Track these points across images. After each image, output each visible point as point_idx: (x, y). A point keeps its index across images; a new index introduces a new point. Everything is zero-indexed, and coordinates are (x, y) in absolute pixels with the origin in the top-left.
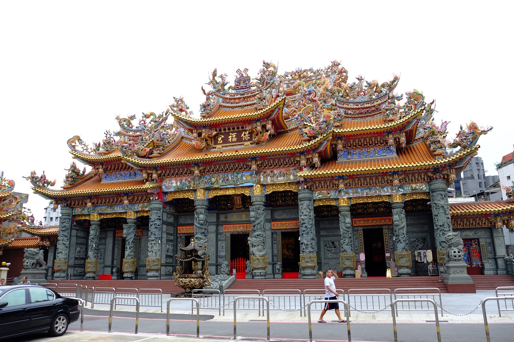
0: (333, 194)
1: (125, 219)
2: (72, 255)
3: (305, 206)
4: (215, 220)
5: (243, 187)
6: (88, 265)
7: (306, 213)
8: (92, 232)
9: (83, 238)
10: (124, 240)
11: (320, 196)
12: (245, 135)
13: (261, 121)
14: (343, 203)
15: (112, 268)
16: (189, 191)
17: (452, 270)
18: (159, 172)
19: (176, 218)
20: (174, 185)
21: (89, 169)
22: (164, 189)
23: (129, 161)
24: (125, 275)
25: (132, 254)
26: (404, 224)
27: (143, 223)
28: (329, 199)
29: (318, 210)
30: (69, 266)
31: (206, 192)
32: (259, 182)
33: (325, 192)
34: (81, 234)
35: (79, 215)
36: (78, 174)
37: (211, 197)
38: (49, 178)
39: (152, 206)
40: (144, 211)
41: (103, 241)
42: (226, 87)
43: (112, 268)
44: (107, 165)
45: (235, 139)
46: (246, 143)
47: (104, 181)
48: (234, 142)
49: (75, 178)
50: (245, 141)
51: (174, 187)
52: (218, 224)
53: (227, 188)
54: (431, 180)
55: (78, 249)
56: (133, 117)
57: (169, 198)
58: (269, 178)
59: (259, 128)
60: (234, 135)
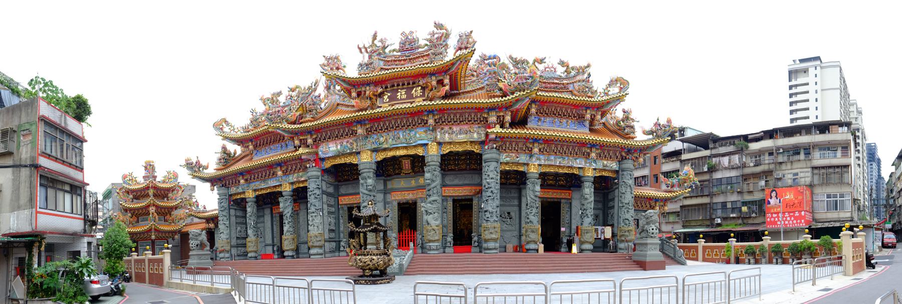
0: (523, 158)
1: (281, 193)
2: (234, 235)
3: (492, 168)
4: (382, 188)
5: (415, 146)
6: (248, 244)
7: (491, 176)
8: (249, 210)
9: (243, 217)
10: (281, 217)
14: (533, 170)
15: (273, 246)
16: (351, 154)
17: (649, 246)
19: (337, 188)
22: (321, 155)
23: (278, 128)
24: (286, 254)
25: (291, 229)
26: (592, 199)
27: (300, 195)
28: (518, 164)
29: (505, 175)
30: (231, 247)
31: (374, 154)
32: (435, 140)
34: (239, 213)
35: (235, 194)
36: (229, 155)
37: (379, 159)
38: (203, 163)
39: (310, 174)
40: (299, 182)
41: (262, 219)
42: (387, 51)
43: (273, 246)
44: (256, 140)
45: (404, 97)
46: (418, 100)
47: (255, 158)
49: (227, 159)
50: (417, 97)
52: (386, 192)
53: (397, 148)
55: (239, 228)
56: (279, 94)
57: (327, 165)
59: (434, 83)
60: (403, 92)
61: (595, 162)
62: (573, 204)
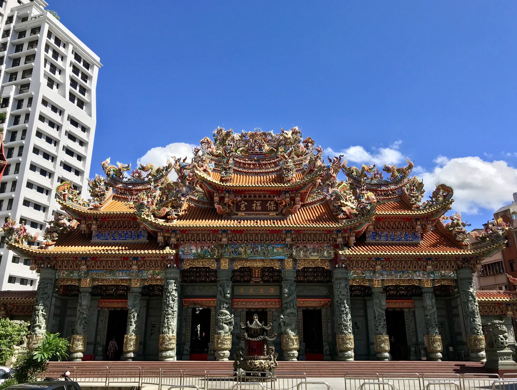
0: (368, 275)
11: (355, 275)
12: (270, 204)
13: (290, 192)
14: (377, 285)
18: (178, 236)
20: (194, 251)
21: (74, 223)
33: (360, 272)
45: (259, 208)
46: (271, 214)
48: (259, 211)
50: (270, 211)
51: (194, 254)
54: (459, 267)
58: (302, 252)
61: (432, 273)
62: (416, 312)
